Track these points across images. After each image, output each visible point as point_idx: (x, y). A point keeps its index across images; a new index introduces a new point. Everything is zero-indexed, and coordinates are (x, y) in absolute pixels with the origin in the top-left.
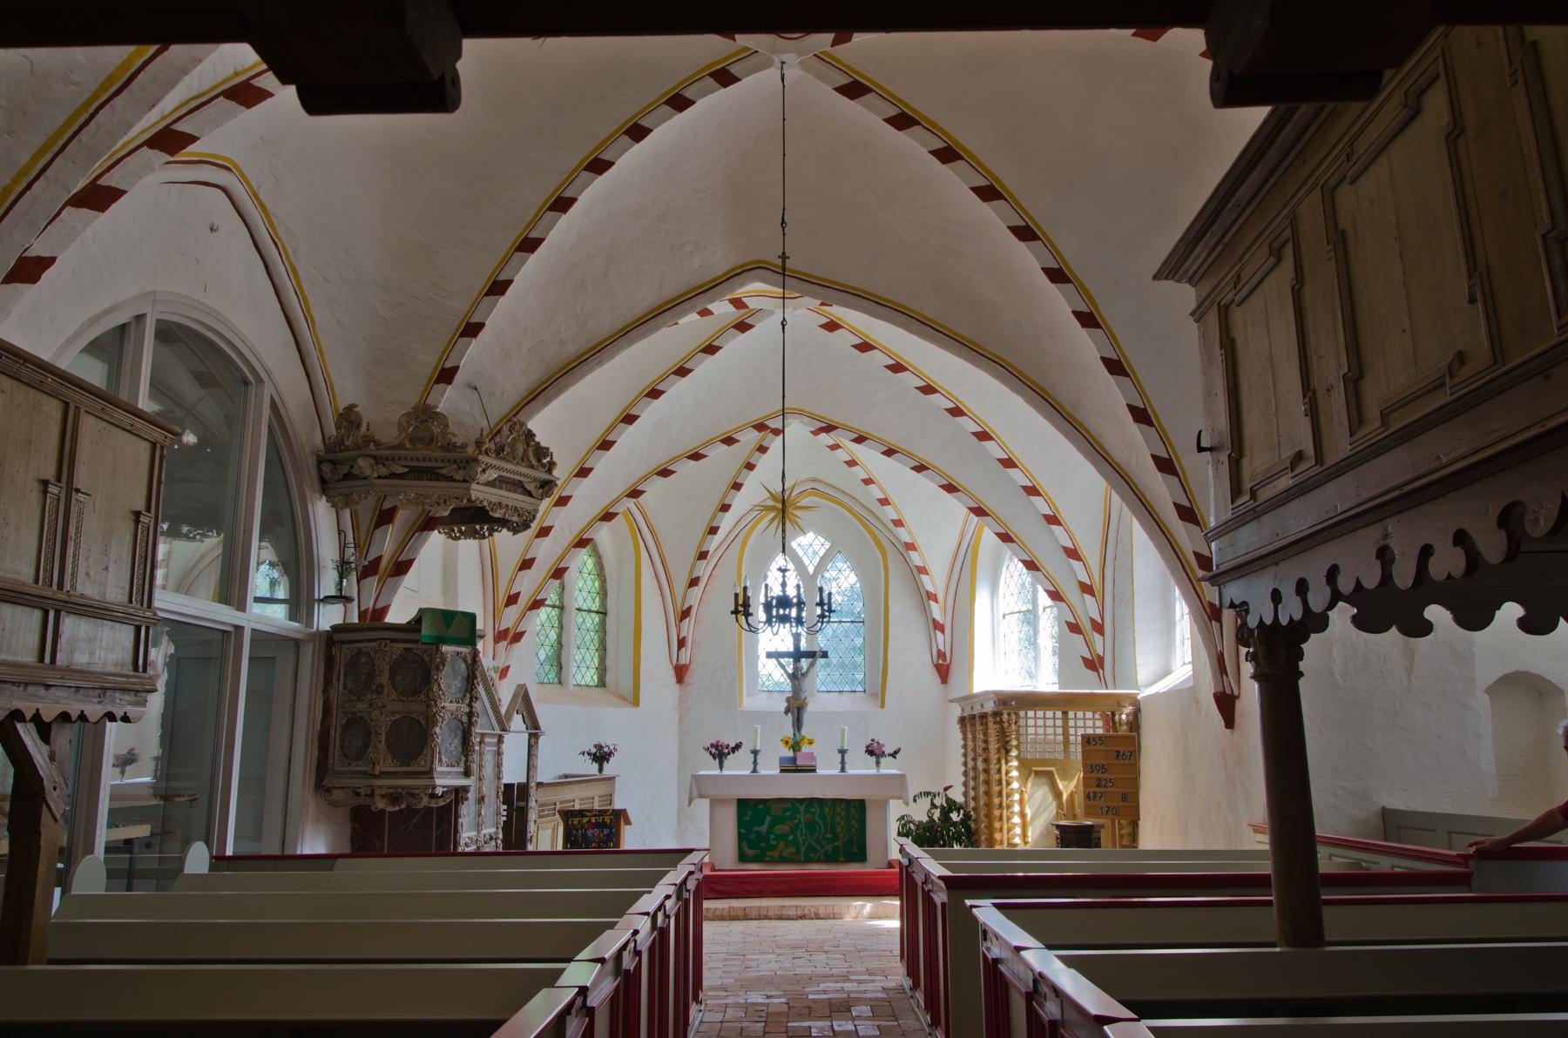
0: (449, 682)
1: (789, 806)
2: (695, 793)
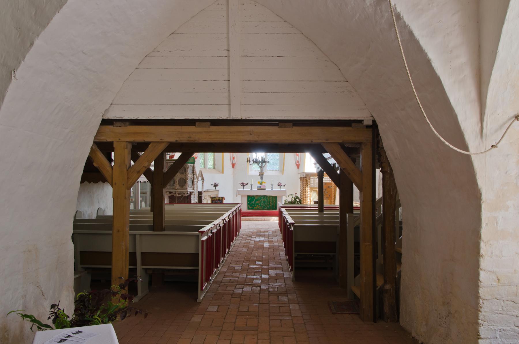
1: (259, 197)
2: (238, 194)
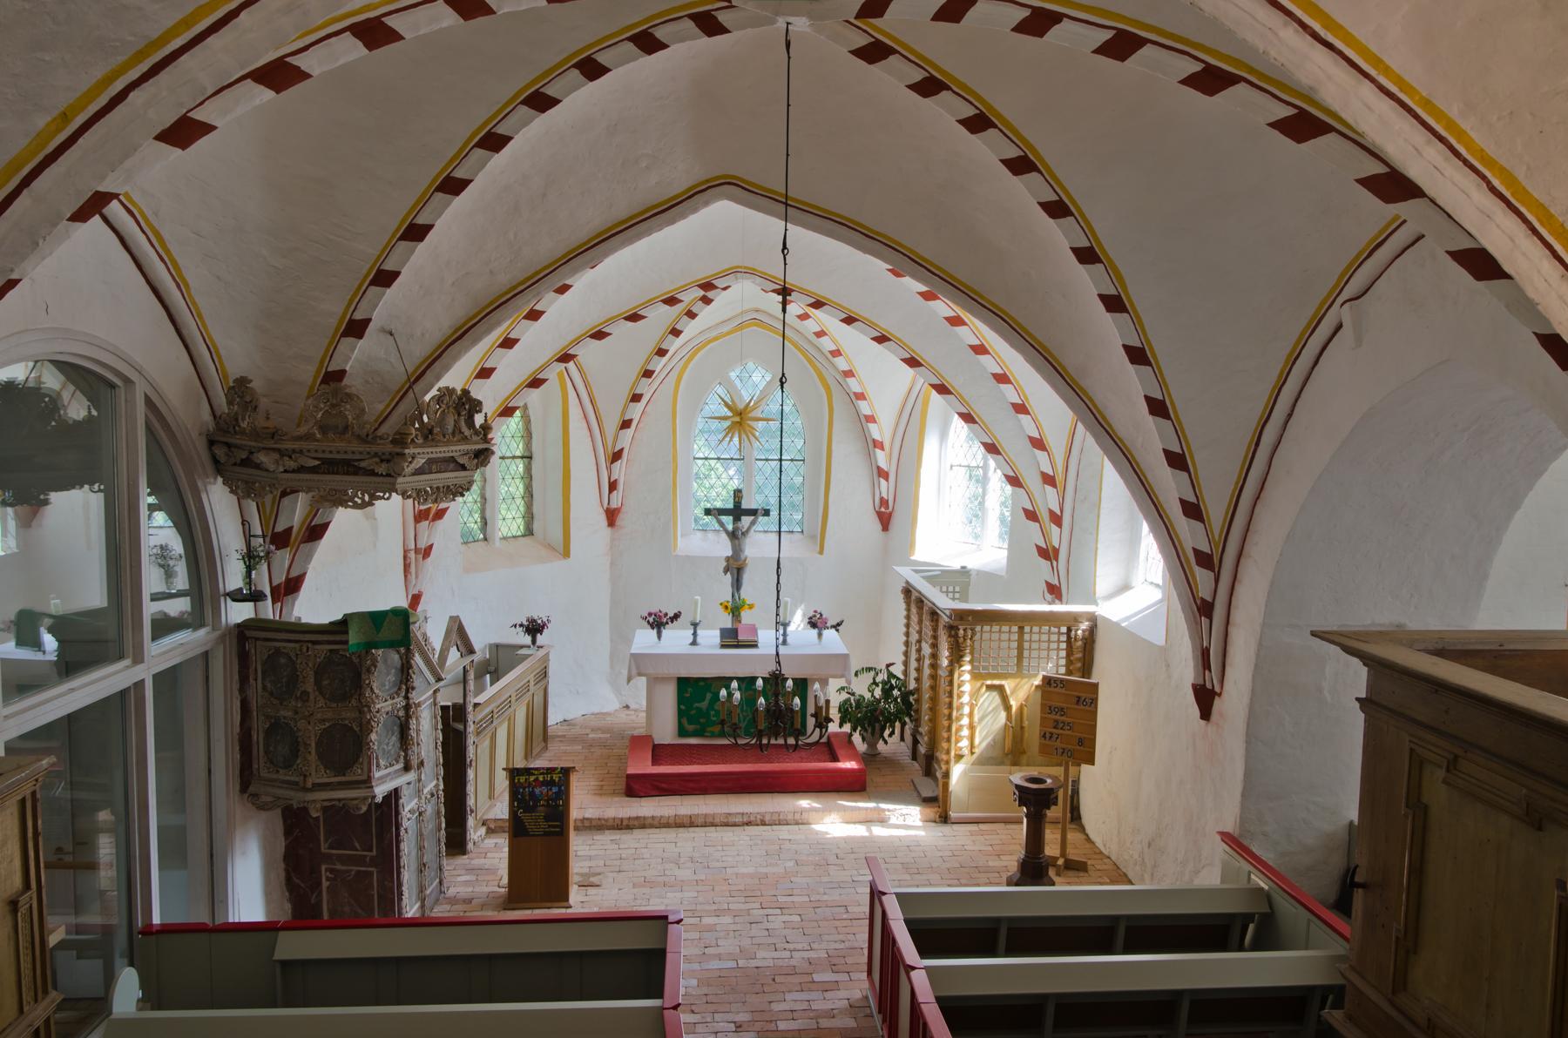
0: (381, 682)
2: (634, 672)
